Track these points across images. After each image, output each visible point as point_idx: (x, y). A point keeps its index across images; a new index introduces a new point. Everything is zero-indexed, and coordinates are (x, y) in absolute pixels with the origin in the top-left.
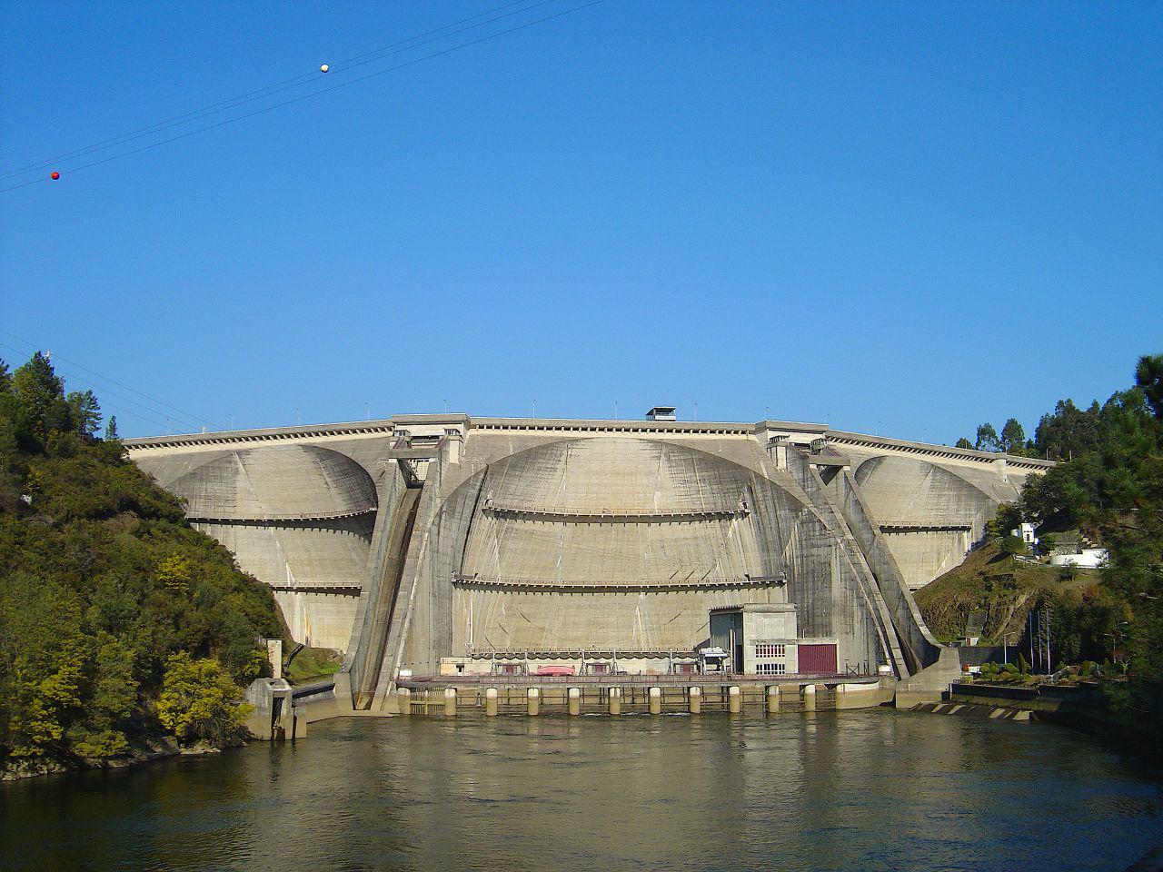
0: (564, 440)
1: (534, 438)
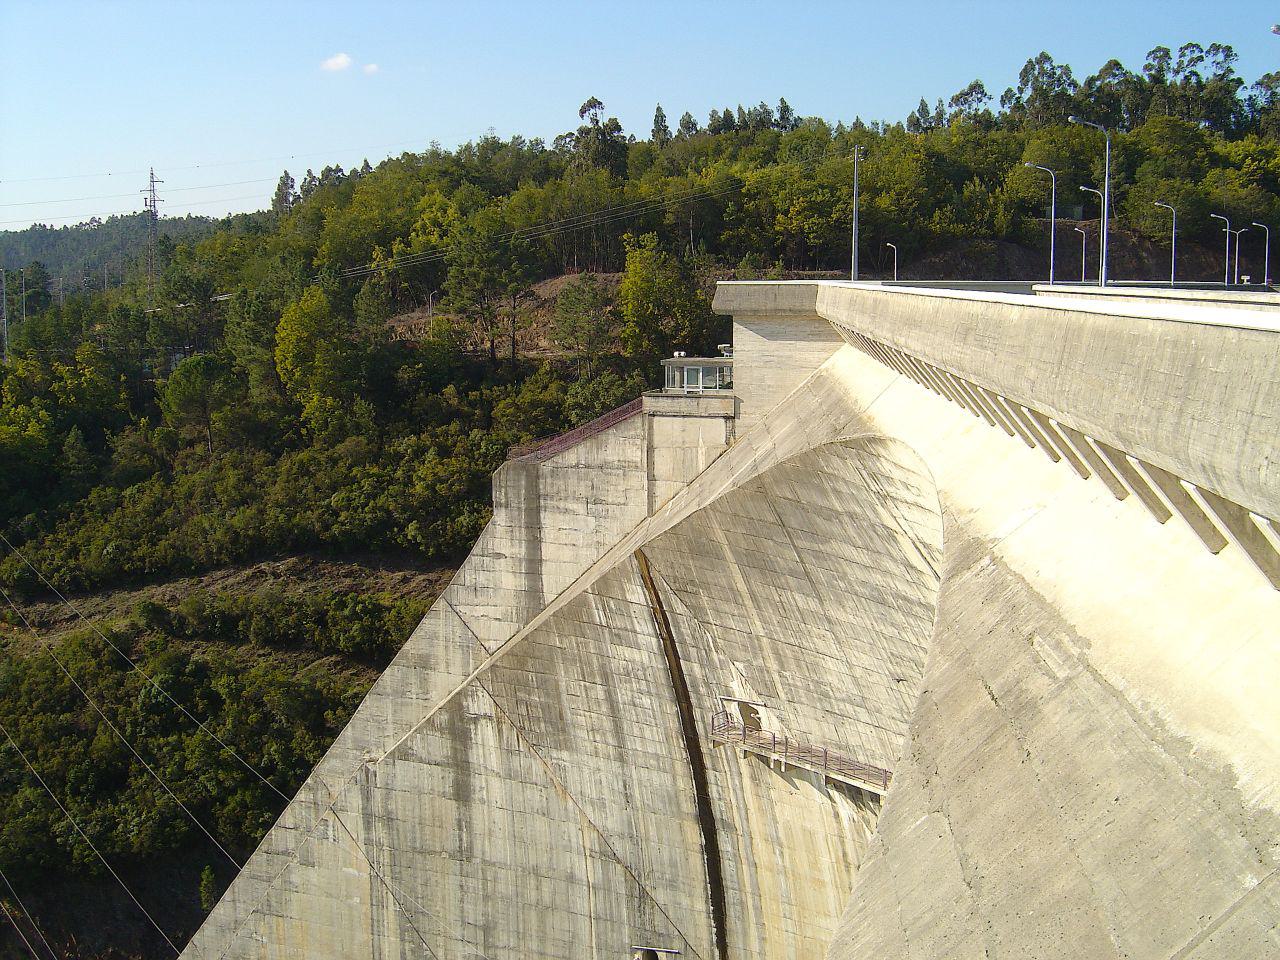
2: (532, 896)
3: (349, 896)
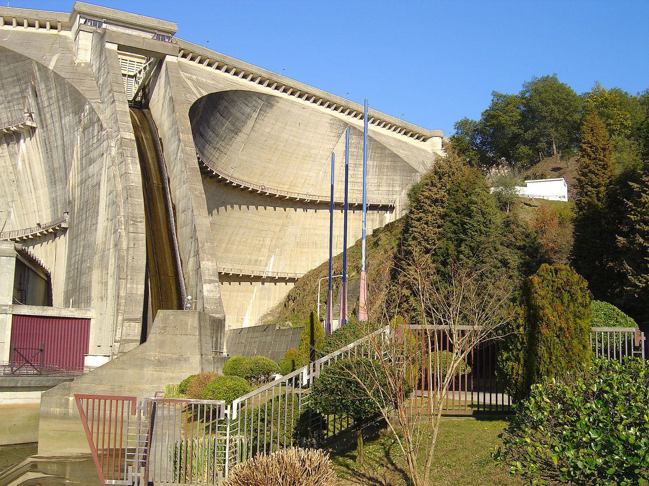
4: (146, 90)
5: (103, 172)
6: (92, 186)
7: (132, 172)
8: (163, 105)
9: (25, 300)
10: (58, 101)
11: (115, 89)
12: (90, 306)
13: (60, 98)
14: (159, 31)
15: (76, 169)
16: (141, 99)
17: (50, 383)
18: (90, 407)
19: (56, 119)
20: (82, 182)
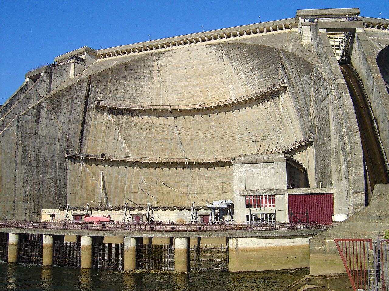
0: (152, 55)
1: (133, 56)
2: (48, 142)
3: (12, 143)
4: (347, 52)
5: (330, 106)
6: (324, 115)
7: (347, 103)
8: (359, 59)
9: (294, 185)
10: (297, 69)
11: (329, 55)
12: (332, 186)
13: (298, 67)
14: (349, 15)
15: (313, 106)
16: (345, 58)
17: (314, 233)
18: (344, 246)
19: (297, 79)
20: (318, 114)
